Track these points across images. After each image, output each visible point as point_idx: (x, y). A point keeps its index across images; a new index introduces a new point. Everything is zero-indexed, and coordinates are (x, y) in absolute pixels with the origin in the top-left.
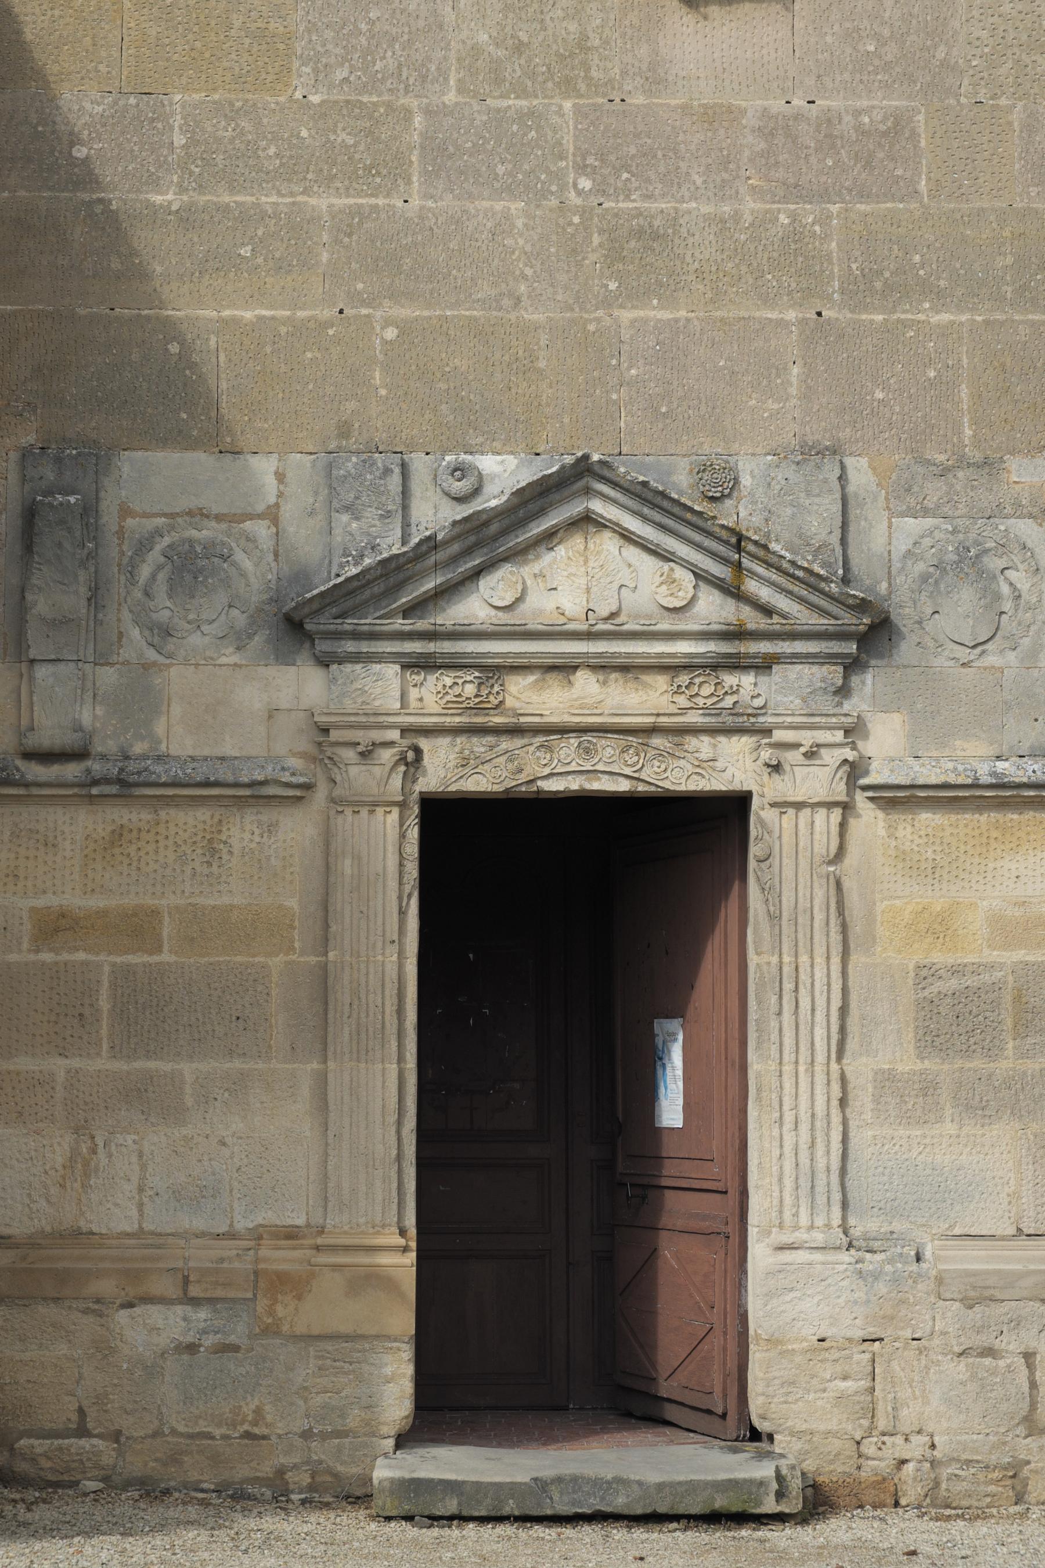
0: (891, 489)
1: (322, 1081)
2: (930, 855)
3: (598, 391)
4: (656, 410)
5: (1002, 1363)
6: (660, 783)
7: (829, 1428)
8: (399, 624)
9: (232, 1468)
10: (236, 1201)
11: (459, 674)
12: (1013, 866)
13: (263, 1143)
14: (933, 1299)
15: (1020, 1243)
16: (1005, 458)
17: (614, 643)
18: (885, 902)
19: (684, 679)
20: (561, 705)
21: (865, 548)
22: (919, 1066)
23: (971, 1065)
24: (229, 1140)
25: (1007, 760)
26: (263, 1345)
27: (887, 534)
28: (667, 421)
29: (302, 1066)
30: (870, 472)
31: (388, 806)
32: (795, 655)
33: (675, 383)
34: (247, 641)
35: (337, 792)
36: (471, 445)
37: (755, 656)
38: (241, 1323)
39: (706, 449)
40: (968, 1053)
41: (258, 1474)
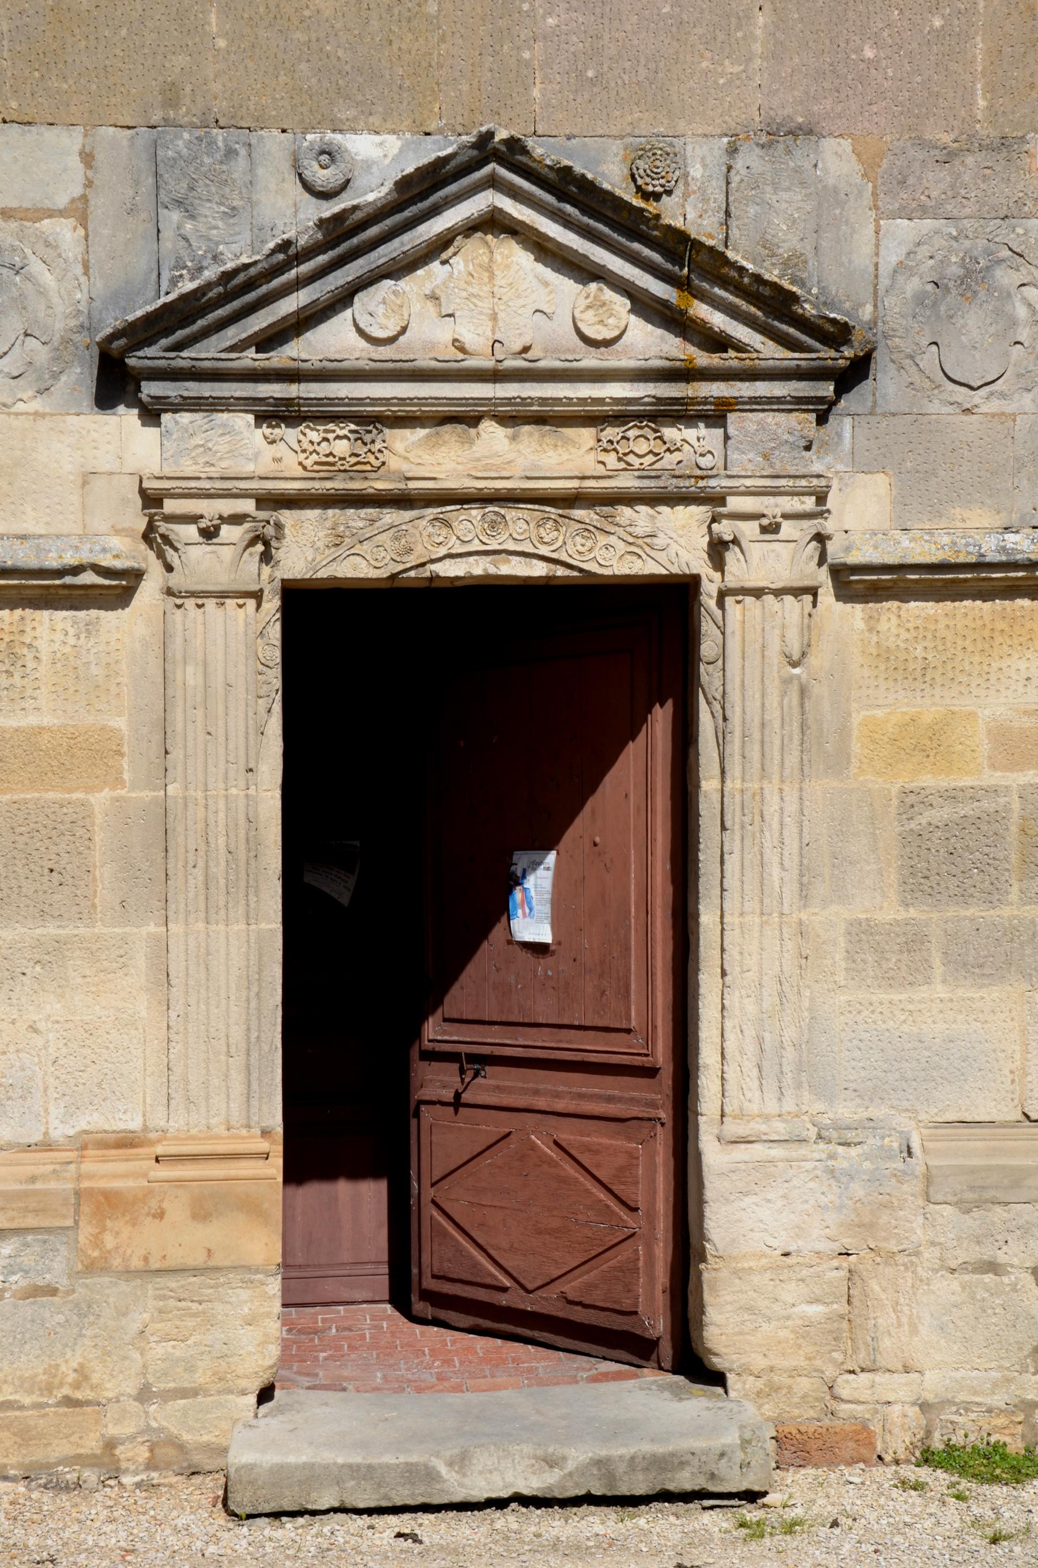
0: (880, 181)
1: (162, 948)
2: (919, 652)
3: (505, 47)
4: (581, 74)
5: (1006, 1280)
6: (584, 566)
7: (794, 1364)
8: (250, 358)
9: (46, 1445)
10: (52, 1102)
11: (331, 426)
12: (1023, 665)
13: (87, 1027)
14: (921, 1202)
15: (1025, 1130)
16: (1028, 137)
17: (528, 385)
18: (863, 713)
19: (611, 432)
20: (460, 467)
21: (844, 259)
22: (902, 915)
23: (968, 913)
24: (41, 1026)
25: (1017, 532)
26: (87, 1286)
27: (873, 241)
28: (595, 90)
29: (135, 930)
30: (854, 158)
31: (241, 597)
32: (754, 400)
33: (607, 36)
34: (50, 382)
35: (175, 580)
36: (341, 121)
37: (705, 401)
38: (59, 1258)
39: (644, 129)
40: (964, 897)
41: (81, 1451)
